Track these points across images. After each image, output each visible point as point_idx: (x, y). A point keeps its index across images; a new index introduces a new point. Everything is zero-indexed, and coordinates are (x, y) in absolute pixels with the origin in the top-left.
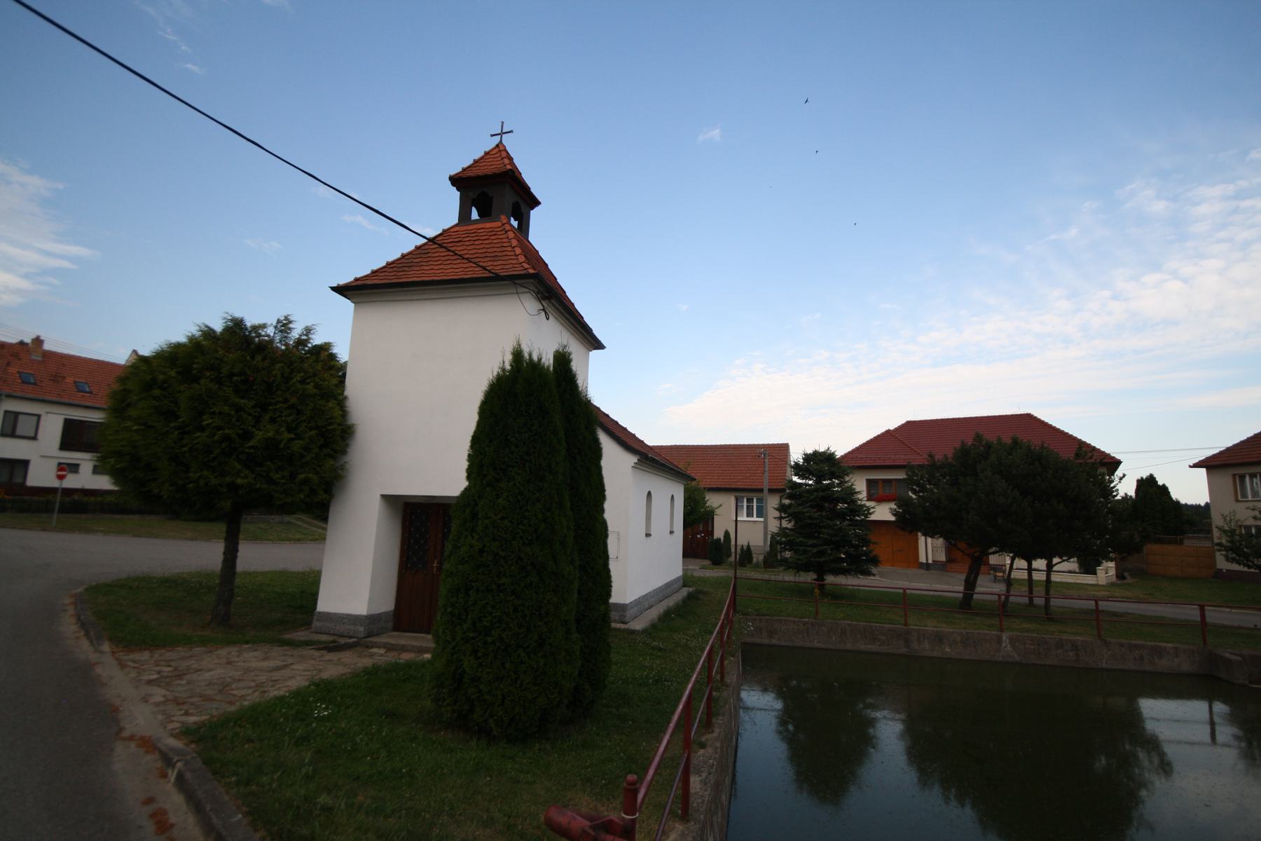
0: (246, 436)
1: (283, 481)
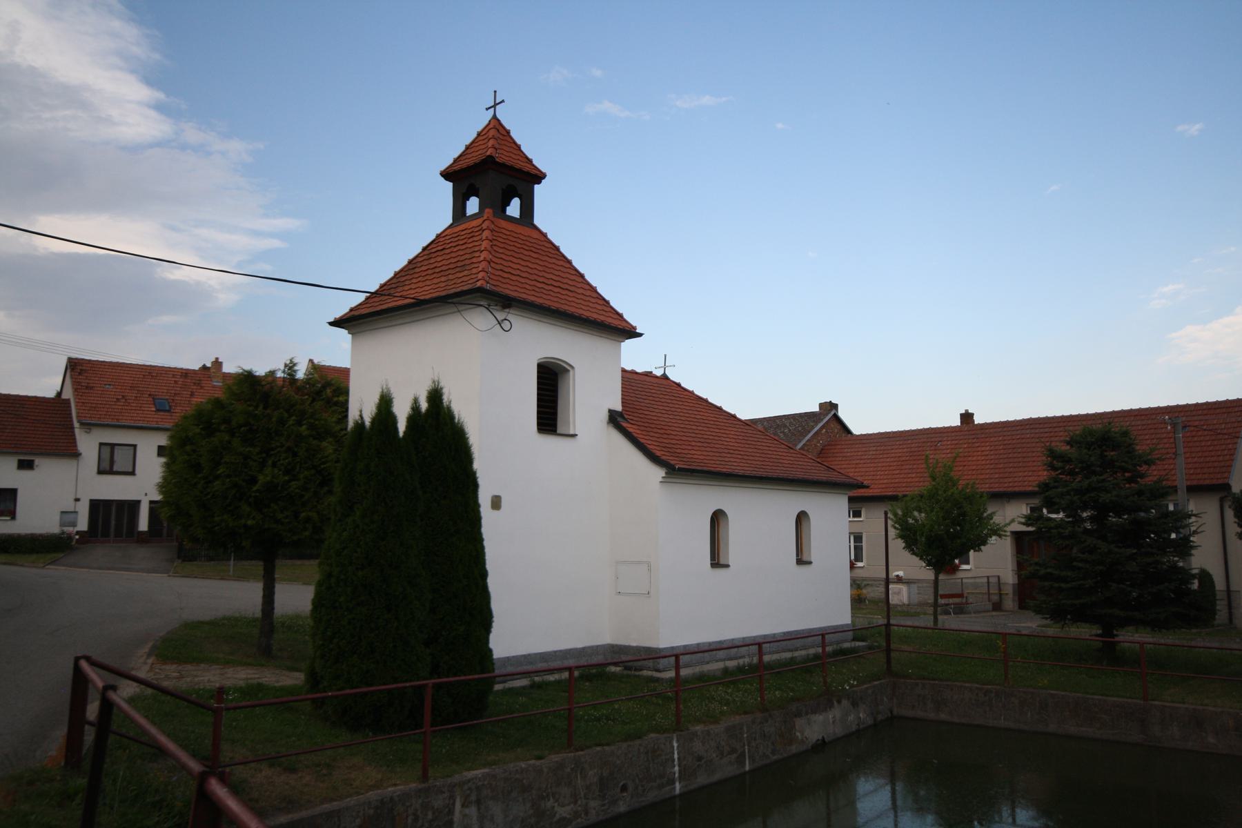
0: (254, 480)
1: (287, 520)
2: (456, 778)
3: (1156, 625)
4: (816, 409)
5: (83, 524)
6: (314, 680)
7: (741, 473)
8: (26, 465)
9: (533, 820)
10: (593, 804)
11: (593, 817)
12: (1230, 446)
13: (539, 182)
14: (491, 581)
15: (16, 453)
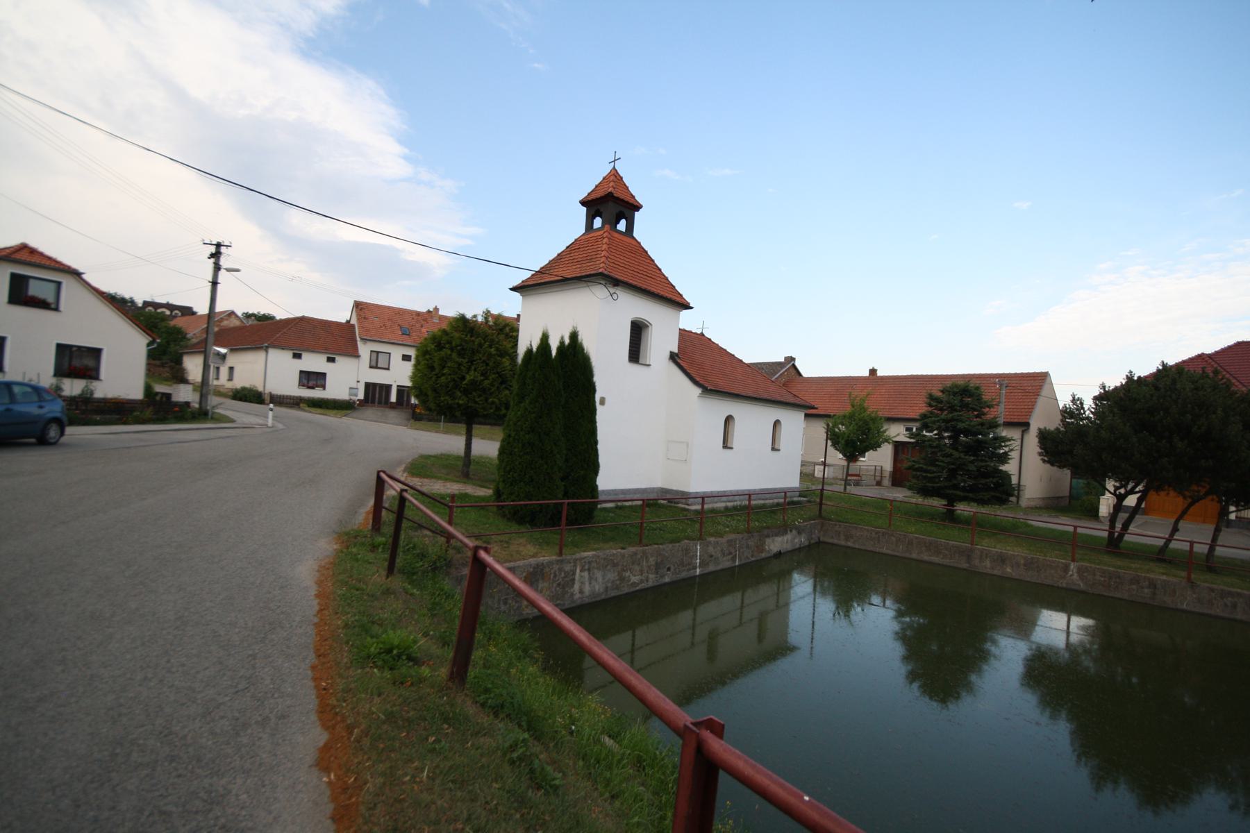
0: (463, 378)
2: (578, 556)
3: (982, 502)
4: (783, 360)
5: (361, 396)
6: (498, 494)
7: (745, 394)
8: (331, 360)
9: (618, 582)
10: (651, 576)
11: (650, 584)
12: (1033, 400)
13: (638, 211)
14: (599, 447)
15: (326, 353)
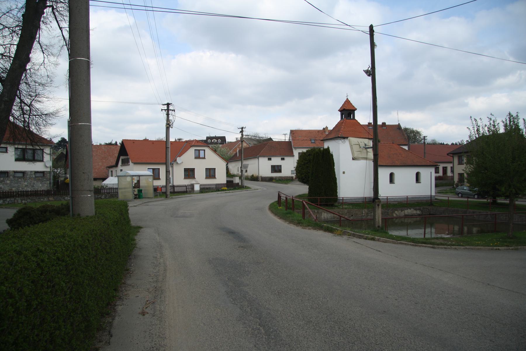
8: (283, 159)
15: (268, 157)
